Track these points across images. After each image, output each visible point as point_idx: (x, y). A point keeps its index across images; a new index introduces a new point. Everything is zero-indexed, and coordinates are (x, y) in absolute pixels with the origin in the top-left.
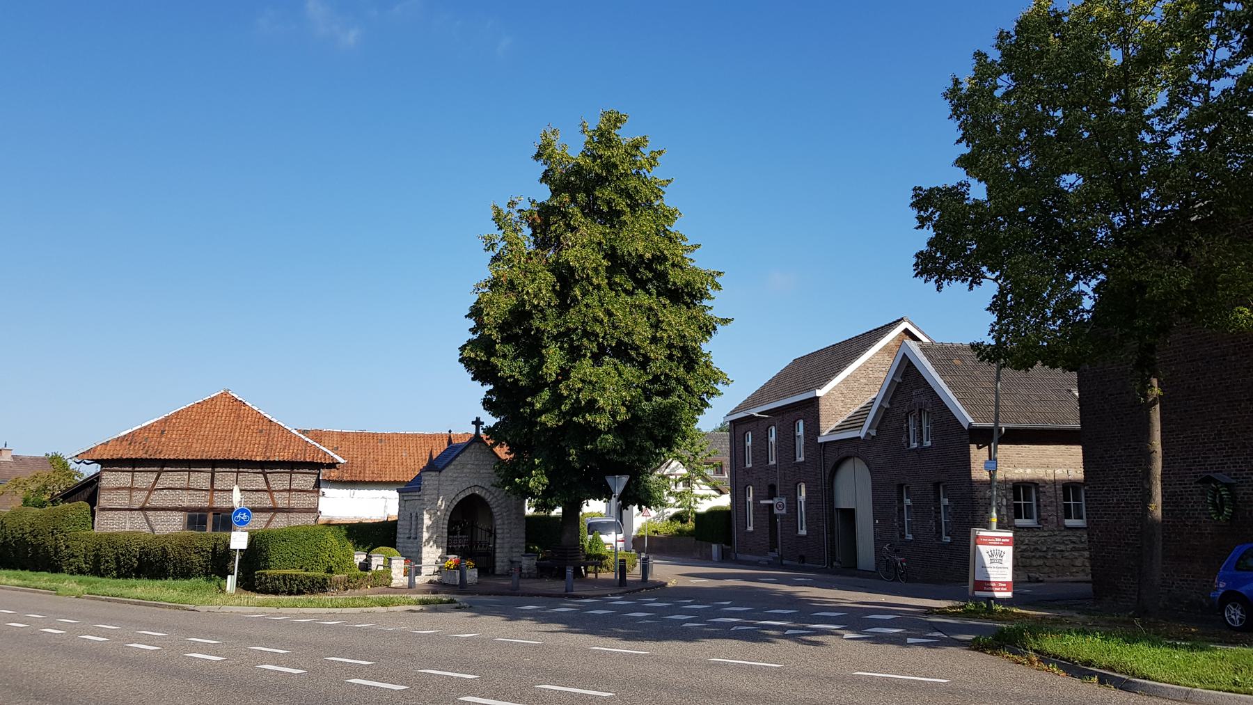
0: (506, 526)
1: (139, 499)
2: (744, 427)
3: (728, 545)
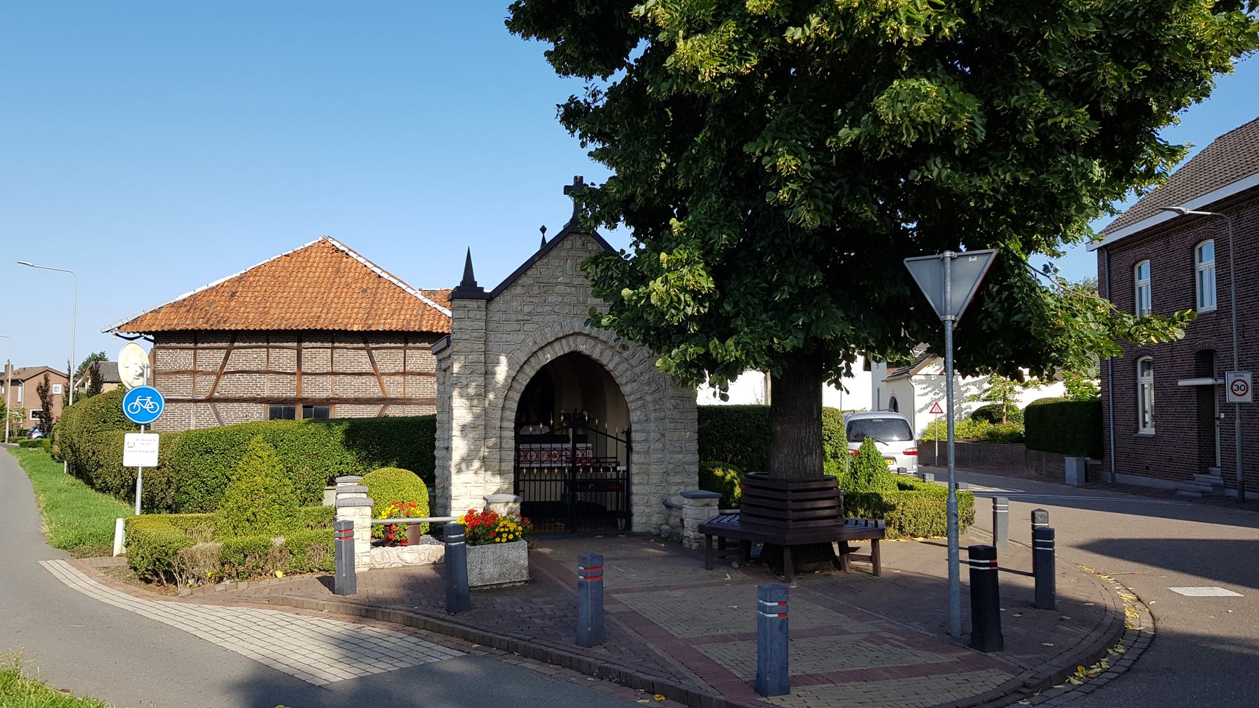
0: (652, 426)
1: (204, 386)
2: (1130, 255)
3: (1096, 458)
